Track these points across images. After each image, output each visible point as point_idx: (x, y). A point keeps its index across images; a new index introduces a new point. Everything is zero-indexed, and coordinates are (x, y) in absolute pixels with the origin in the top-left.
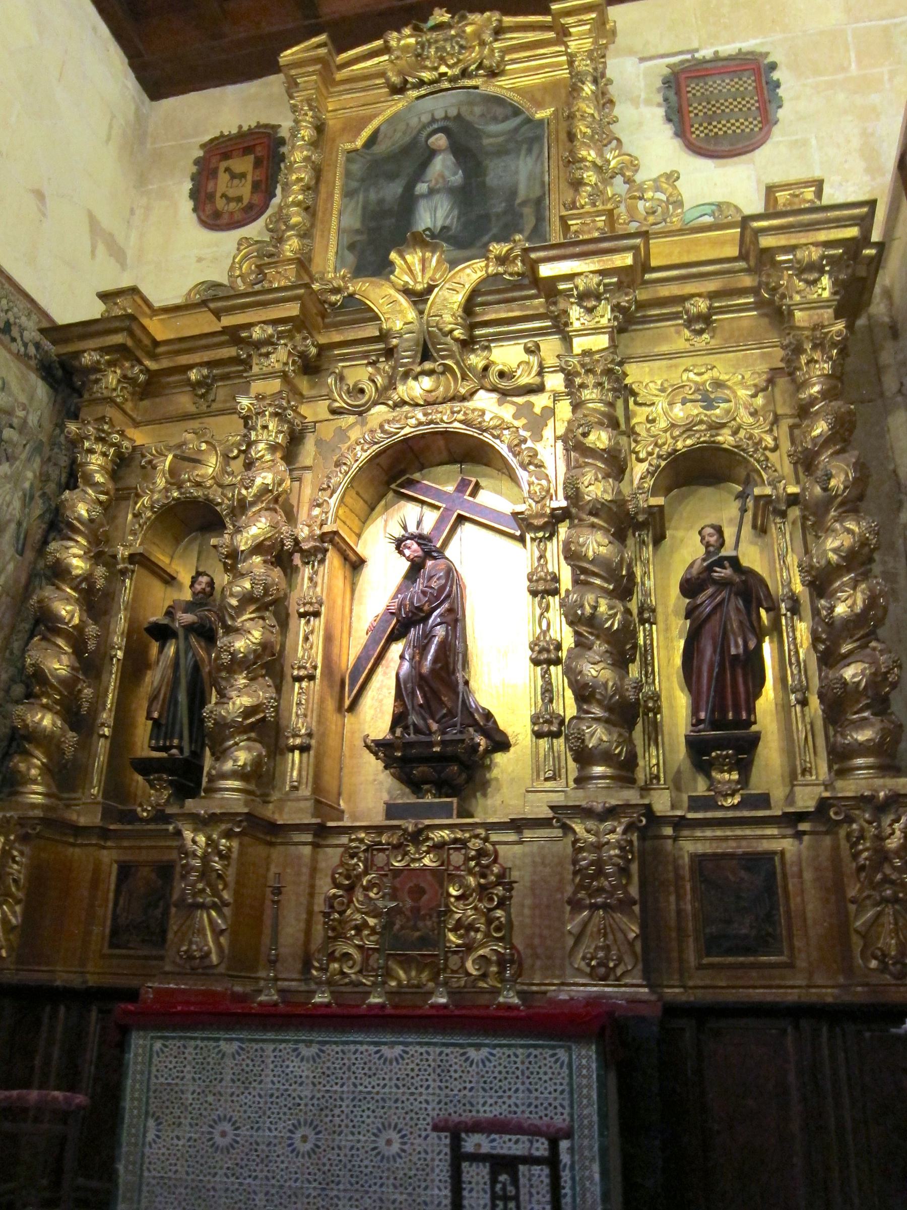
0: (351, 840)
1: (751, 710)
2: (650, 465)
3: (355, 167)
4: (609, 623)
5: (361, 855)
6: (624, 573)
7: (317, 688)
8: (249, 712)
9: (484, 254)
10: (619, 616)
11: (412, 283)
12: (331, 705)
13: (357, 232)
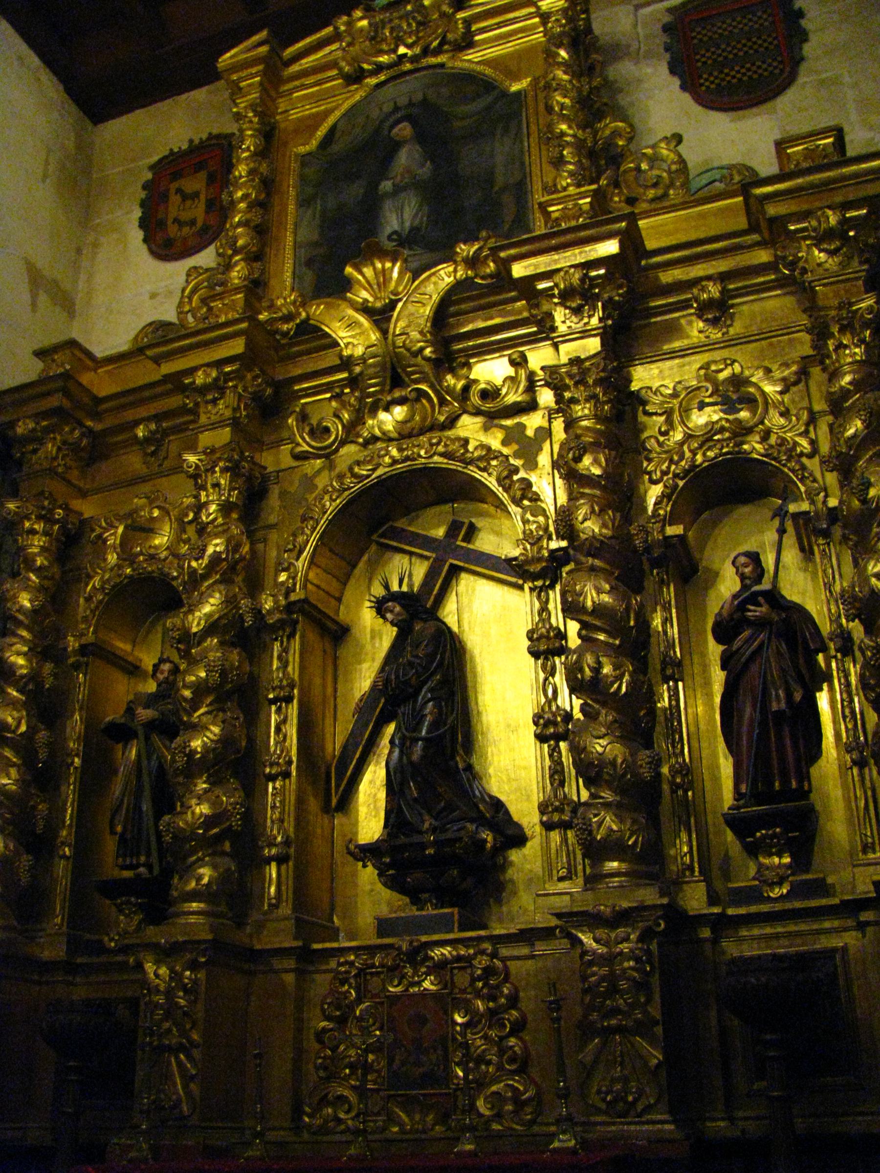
0: (340, 964)
1: (804, 776)
2: (665, 486)
3: (309, 171)
4: (616, 686)
5: (352, 981)
6: (632, 623)
7: (293, 787)
8: (209, 821)
9: (450, 258)
10: (627, 677)
11: (371, 299)
12: (313, 805)
13: (316, 244)
